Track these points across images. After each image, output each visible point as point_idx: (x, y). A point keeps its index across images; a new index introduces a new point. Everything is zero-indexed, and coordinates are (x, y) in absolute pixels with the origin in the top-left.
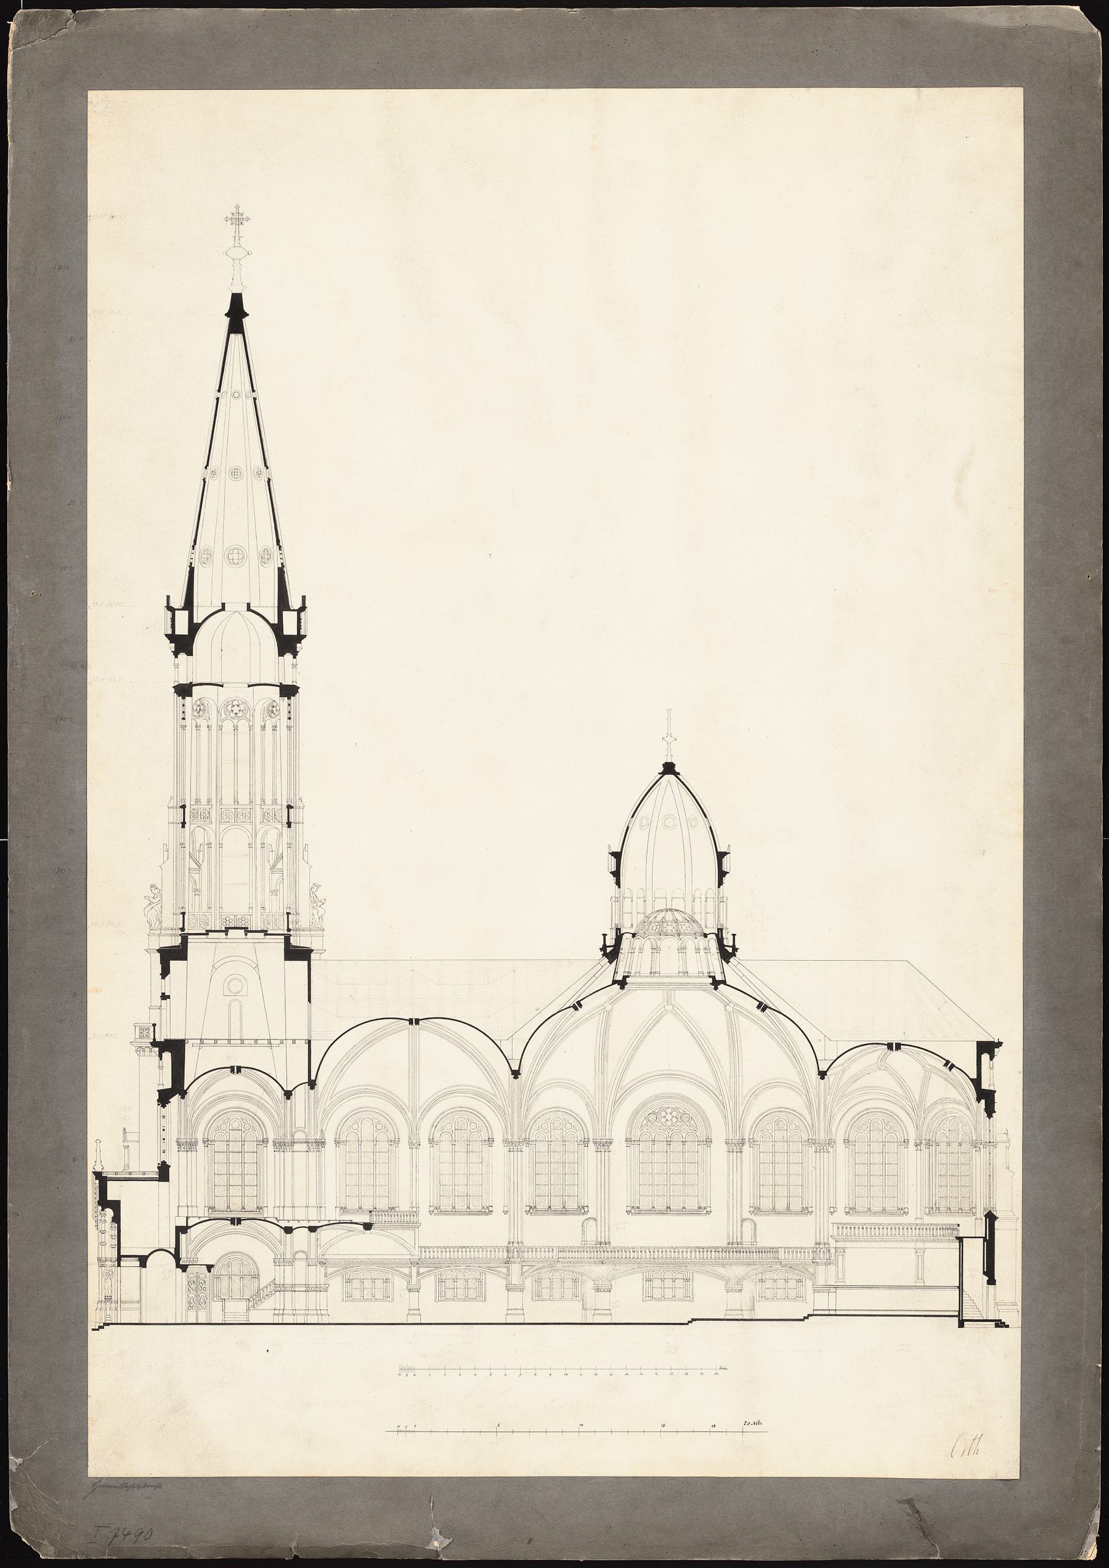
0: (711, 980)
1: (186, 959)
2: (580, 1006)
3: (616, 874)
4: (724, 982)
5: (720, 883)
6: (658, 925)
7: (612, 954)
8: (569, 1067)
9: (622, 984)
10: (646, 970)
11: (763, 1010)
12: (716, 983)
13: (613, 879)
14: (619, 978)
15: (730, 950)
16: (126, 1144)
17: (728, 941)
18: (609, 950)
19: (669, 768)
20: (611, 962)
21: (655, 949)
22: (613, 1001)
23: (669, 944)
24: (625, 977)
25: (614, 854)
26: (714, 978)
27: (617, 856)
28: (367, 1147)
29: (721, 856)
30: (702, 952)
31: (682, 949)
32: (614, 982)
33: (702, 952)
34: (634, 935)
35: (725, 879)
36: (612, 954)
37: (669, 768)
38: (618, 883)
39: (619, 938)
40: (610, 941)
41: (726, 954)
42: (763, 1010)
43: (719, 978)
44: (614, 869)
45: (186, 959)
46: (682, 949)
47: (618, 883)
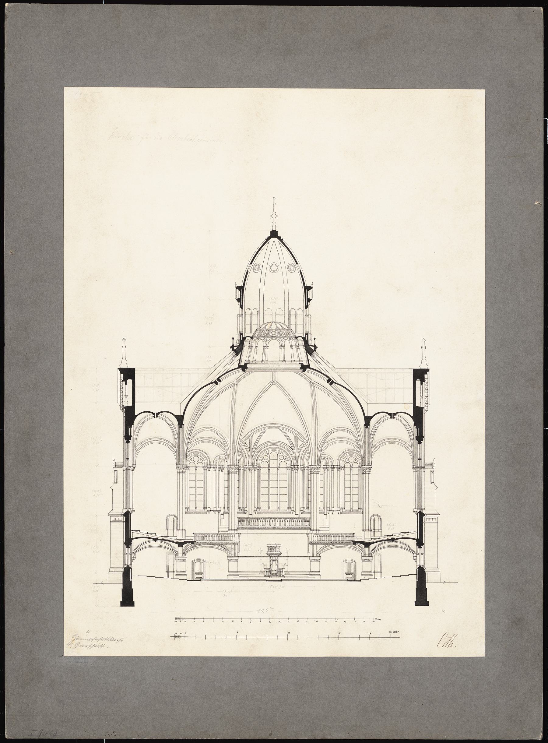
0: (300, 366)
1: (414, 370)
2: (220, 381)
3: (240, 300)
4: (309, 367)
5: (306, 307)
6: (266, 333)
7: (238, 350)
8: (216, 417)
9: (244, 368)
10: (259, 358)
11: (331, 384)
12: (304, 368)
13: (237, 303)
14: (243, 364)
15: (313, 348)
16: (115, 469)
17: (311, 343)
18: (235, 348)
19: (274, 234)
20: (237, 355)
21: (266, 347)
22: (239, 380)
23: (274, 344)
24: (246, 364)
25: (239, 288)
26: (302, 364)
27: (241, 289)
28: (274, 471)
29: (307, 289)
30: (254, 348)
31: (282, 347)
32: (239, 367)
33: (254, 348)
34: (252, 338)
35: (311, 304)
36: (238, 350)
37: (274, 234)
38: (242, 307)
39: (242, 341)
40: (237, 343)
41: (310, 350)
42: (331, 384)
43: (305, 364)
44: (238, 297)
45: (414, 370)
46: (282, 347)
47: (242, 307)
